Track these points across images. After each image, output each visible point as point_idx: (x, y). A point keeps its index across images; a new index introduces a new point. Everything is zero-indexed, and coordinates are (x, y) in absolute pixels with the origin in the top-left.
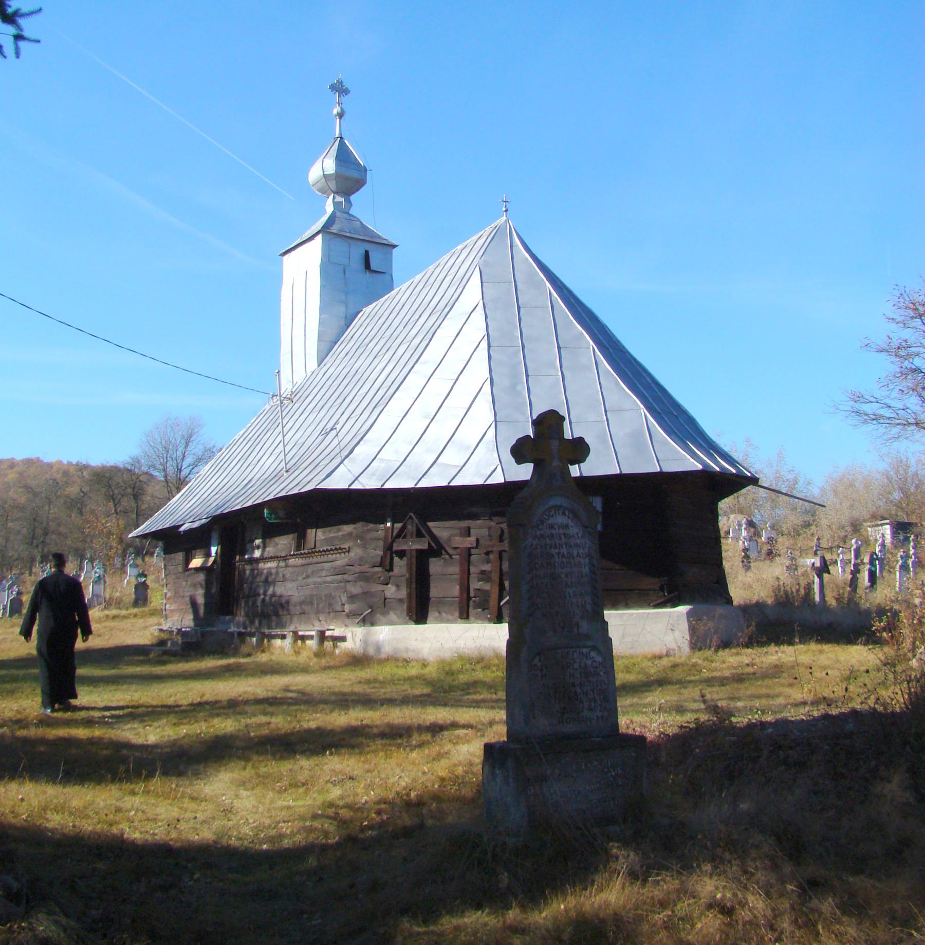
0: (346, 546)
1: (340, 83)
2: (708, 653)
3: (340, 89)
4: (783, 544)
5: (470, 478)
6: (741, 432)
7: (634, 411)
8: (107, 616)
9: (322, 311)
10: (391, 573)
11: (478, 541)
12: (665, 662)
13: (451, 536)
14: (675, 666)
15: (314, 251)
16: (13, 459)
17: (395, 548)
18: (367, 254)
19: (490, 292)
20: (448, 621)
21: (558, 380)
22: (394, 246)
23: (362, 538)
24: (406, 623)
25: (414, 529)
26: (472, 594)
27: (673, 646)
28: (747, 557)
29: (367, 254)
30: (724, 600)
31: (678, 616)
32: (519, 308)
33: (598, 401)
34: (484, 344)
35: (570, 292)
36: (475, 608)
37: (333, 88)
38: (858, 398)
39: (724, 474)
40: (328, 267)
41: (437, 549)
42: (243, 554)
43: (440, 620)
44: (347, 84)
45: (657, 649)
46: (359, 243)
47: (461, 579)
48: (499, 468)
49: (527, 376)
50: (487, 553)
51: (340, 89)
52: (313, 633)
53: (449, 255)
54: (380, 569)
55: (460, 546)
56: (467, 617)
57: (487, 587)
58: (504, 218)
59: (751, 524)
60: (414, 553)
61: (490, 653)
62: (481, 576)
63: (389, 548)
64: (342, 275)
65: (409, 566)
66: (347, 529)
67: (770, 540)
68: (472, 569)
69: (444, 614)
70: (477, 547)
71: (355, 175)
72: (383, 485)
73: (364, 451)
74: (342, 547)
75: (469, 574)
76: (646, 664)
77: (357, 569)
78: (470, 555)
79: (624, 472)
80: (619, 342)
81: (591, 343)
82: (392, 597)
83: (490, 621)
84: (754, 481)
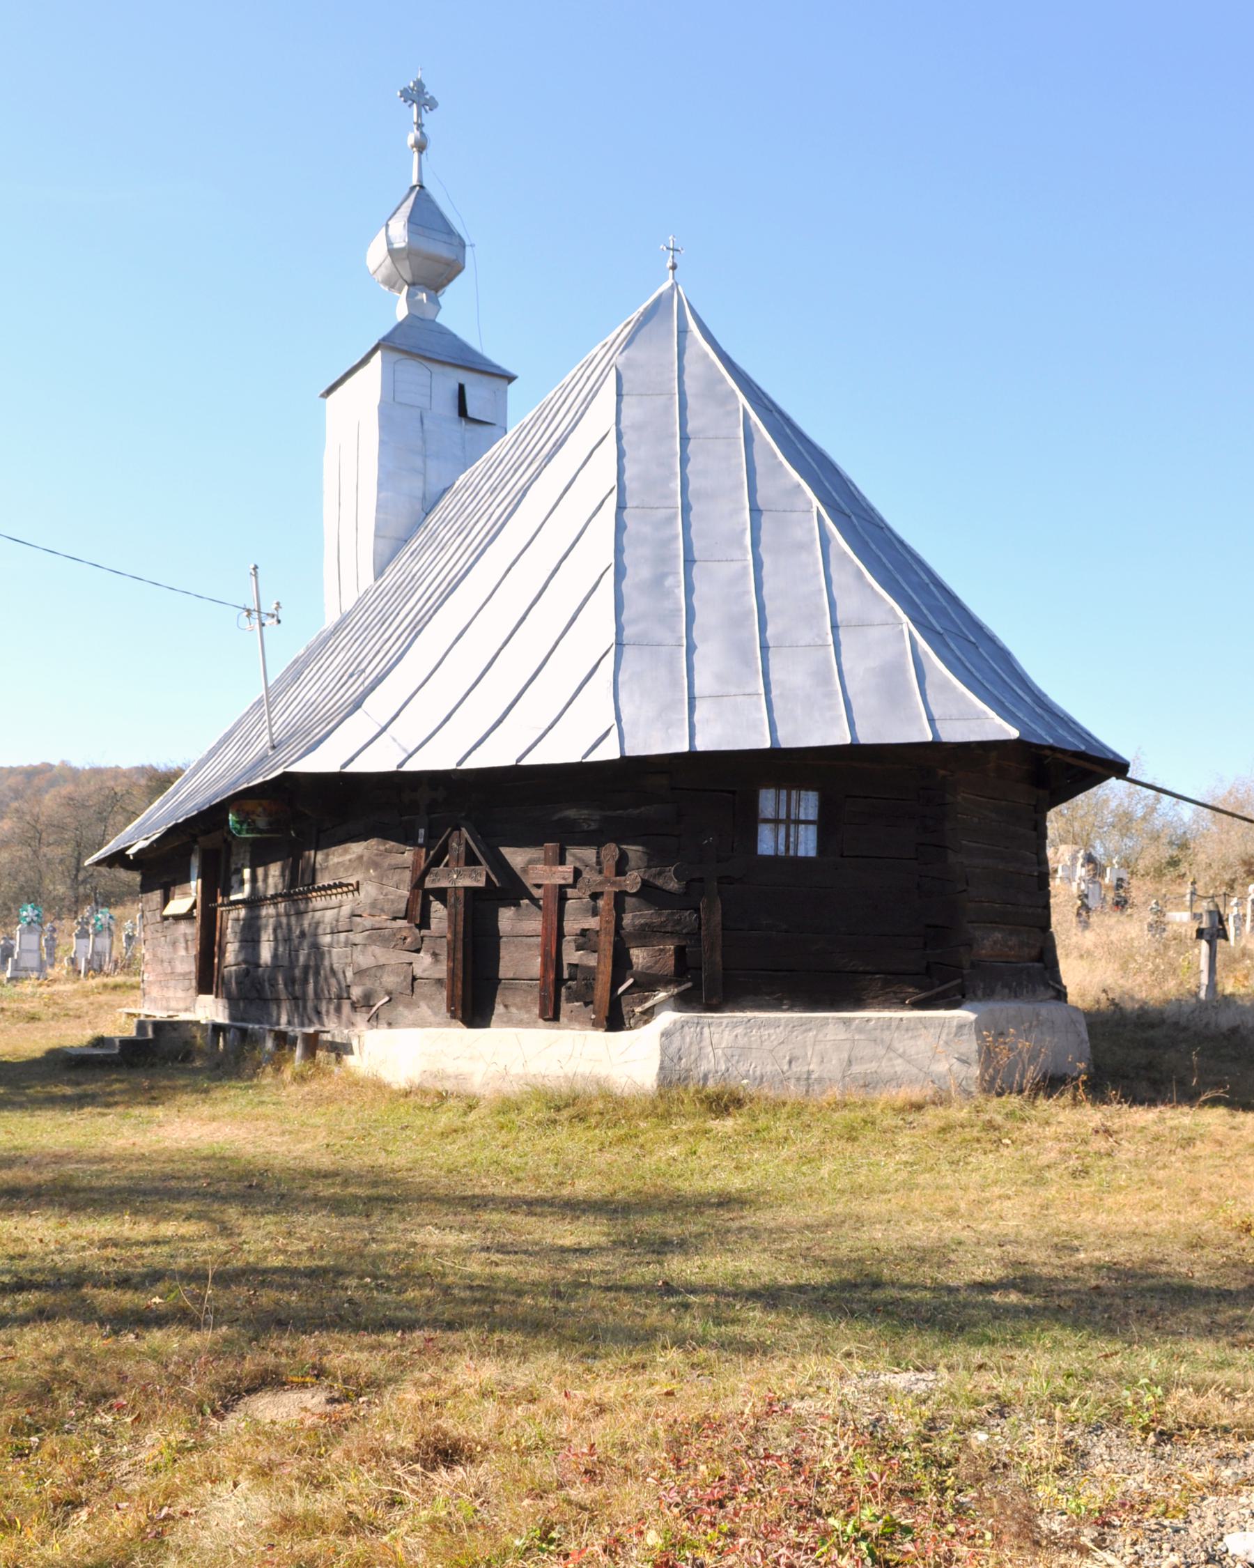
0: (353, 881)
1: (419, 84)
2: (1014, 1101)
3: (418, 96)
4: (1138, 890)
5: (563, 749)
7: (888, 628)
8: (105, 986)
9: (381, 486)
10: (424, 932)
11: (577, 873)
13: (531, 862)
15: (369, 384)
16: (117, 767)
17: (429, 884)
18: (461, 388)
20: (520, 1024)
21: (828, 661)
22: (510, 378)
23: (376, 866)
24: (448, 1025)
25: (462, 848)
26: (566, 976)
28: (1085, 907)
29: (461, 388)
30: (1052, 993)
31: (961, 1027)
34: (613, 498)
35: (788, 420)
36: (569, 1000)
37: (407, 95)
40: (391, 412)
41: (510, 889)
42: (226, 894)
43: (509, 1022)
44: (431, 90)
46: (448, 370)
47: (545, 945)
48: (615, 731)
50: (595, 896)
51: (418, 96)
54: (402, 923)
55: (546, 882)
56: (555, 1018)
57: (591, 960)
58: (670, 282)
59: (1090, 859)
60: (461, 894)
61: (592, 1089)
62: (581, 940)
63: (418, 884)
64: (419, 425)
65: (452, 919)
66: (357, 848)
67: (1120, 883)
68: (572, 925)
69: (513, 1010)
70: (573, 886)
71: (443, 251)
72: (401, 765)
73: (379, 705)
74: (344, 881)
75: (561, 935)
77: (368, 922)
78: (563, 898)
79: (863, 740)
80: (873, 509)
81: (816, 503)
82: (425, 975)
83: (596, 1025)
84: (1119, 768)
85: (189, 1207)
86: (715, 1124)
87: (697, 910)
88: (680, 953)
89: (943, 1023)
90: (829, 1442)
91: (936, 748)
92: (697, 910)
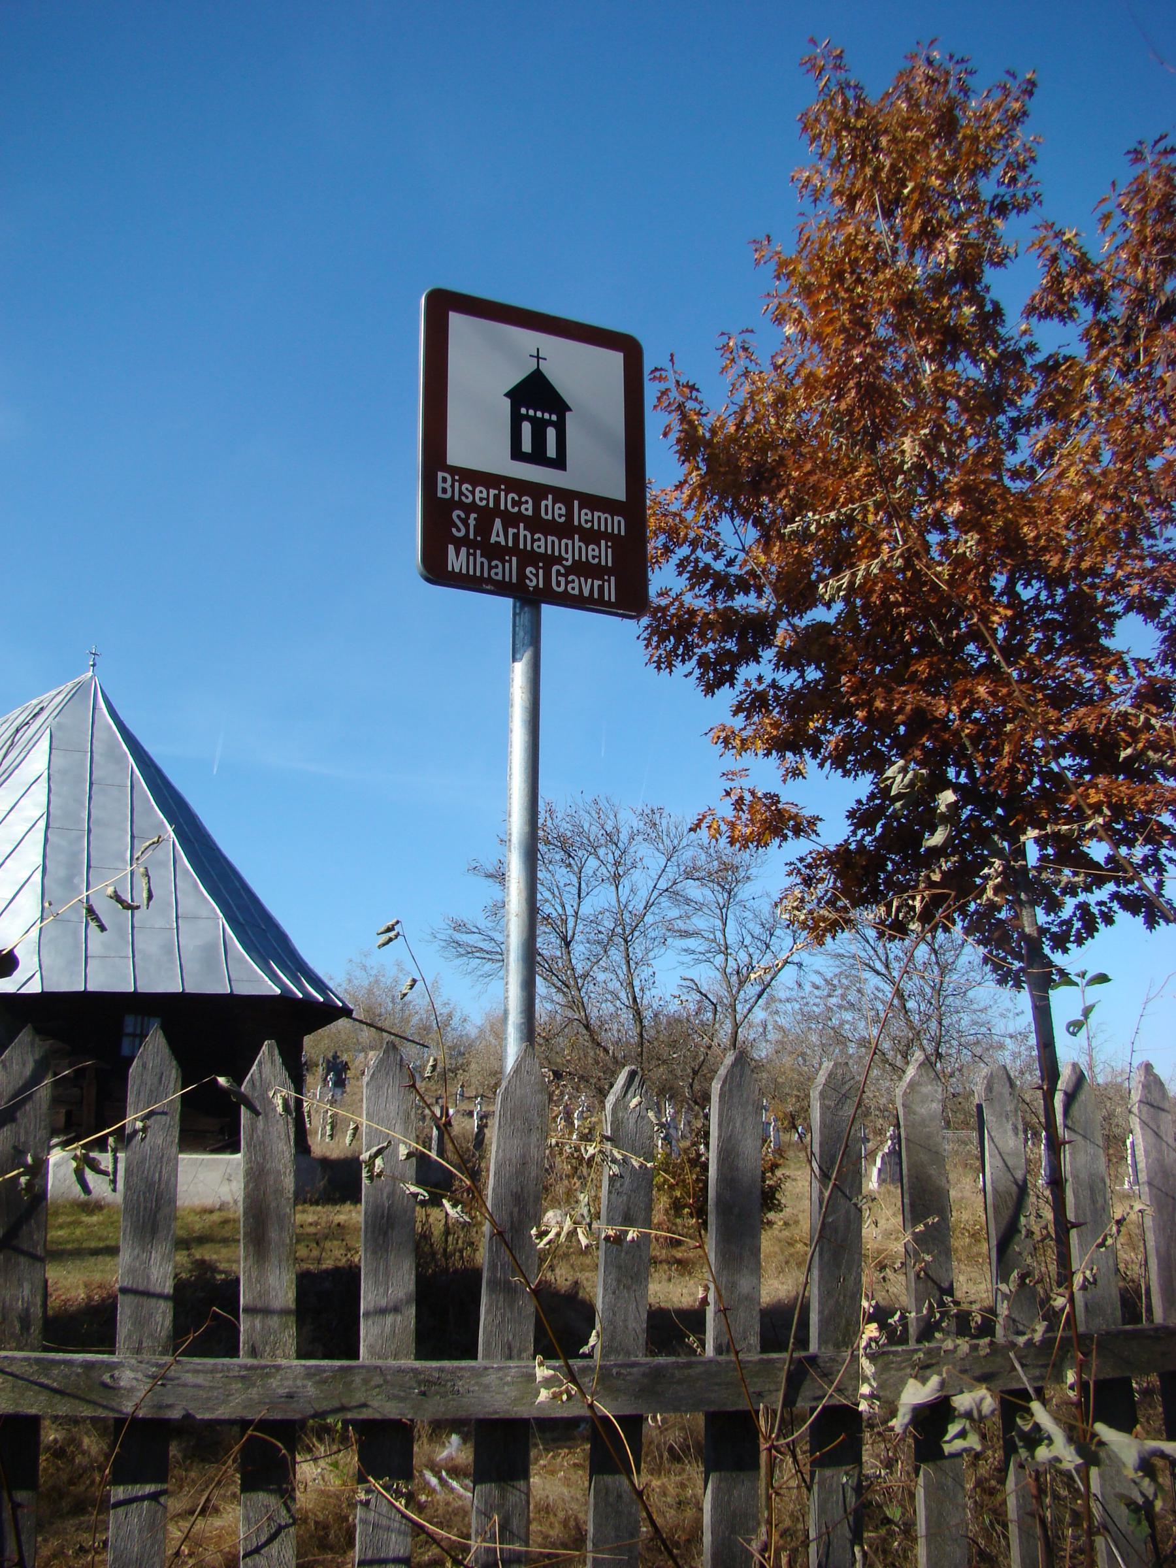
6: (337, 957)
7: (210, 920)
12: (216, 1217)
14: (226, 1222)
19: (58, 761)
27: (228, 1198)
32: (91, 784)
33: (170, 904)
34: (42, 824)
38: (459, 927)
39: (308, 1002)
45: (209, 1201)
48: (38, 975)
49: (89, 867)
52: (813, 1347)
53: (20, 709)
76: (191, 1218)
84: (346, 1012)
85: (69, 1246)
86: (86, 1219)
87: (82, 1088)
88: (69, 1114)
89: (229, 1162)
90: (844, 981)
91: (231, 998)
92: (82, 1088)
